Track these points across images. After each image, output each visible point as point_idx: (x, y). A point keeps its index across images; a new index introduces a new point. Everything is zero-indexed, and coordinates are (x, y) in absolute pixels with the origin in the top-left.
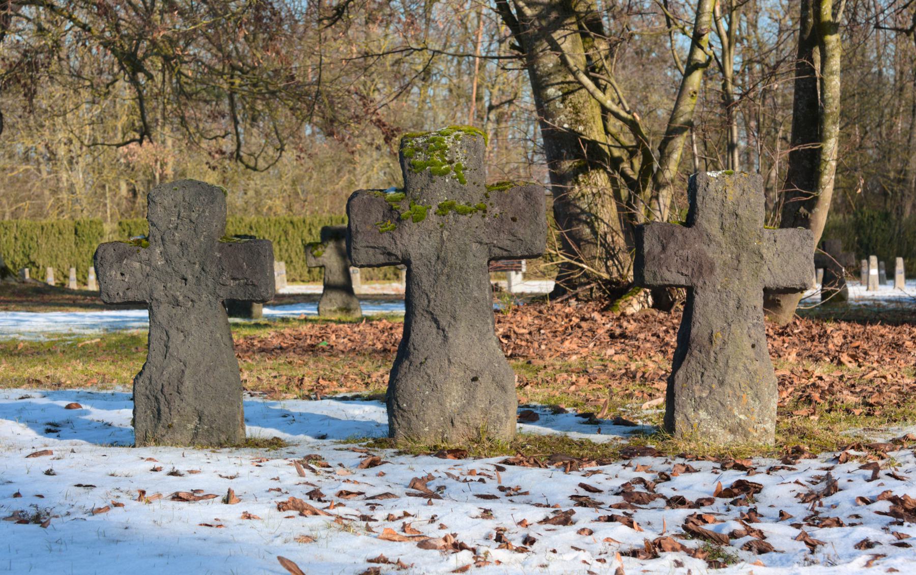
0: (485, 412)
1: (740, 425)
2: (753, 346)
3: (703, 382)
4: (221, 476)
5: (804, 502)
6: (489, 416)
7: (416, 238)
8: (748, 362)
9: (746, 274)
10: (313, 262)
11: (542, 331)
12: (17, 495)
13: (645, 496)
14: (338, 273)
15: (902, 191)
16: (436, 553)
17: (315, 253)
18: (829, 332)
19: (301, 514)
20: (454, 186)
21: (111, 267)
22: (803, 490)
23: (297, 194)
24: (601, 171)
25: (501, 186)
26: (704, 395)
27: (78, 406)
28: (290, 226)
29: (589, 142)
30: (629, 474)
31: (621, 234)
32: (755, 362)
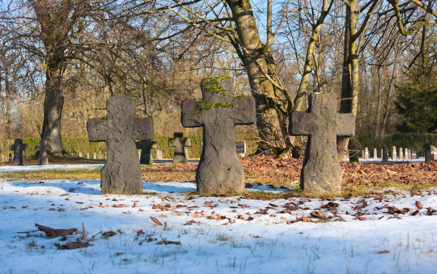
0: (233, 182)
1: (328, 186)
2: (333, 157)
7: (207, 116)
9: (330, 130)
10: (171, 145)
12: (53, 205)
15: (375, 128)
16: (215, 220)
17: (172, 142)
19: (162, 210)
20: (221, 97)
21: (93, 127)
22: (354, 206)
23: (166, 128)
25: (239, 98)
26: (315, 175)
28: (164, 139)
29: (269, 98)
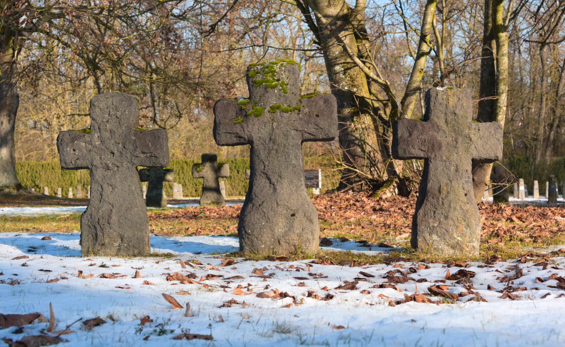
0: (300, 235)
1: (458, 243)
2: (466, 195)
3: (435, 217)
4: (132, 268)
5: (502, 282)
6: (302, 238)
7: (257, 127)
8: (462, 205)
9: (461, 150)
10: (196, 175)
11: (333, 207)
13: (401, 279)
14: (212, 181)
15: (536, 146)
16: (269, 299)
17: (198, 169)
18: (503, 208)
19: (181, 283)
20: (280, 95)
21: (67, 145)
22: (501, 276)
24: (367, 115)
25: (309, 96)
26: (436, 225)
27: (49, 238)
28: (185, 165)
30: (390, 268)
31: (379, 152)
32: (467, 205)
